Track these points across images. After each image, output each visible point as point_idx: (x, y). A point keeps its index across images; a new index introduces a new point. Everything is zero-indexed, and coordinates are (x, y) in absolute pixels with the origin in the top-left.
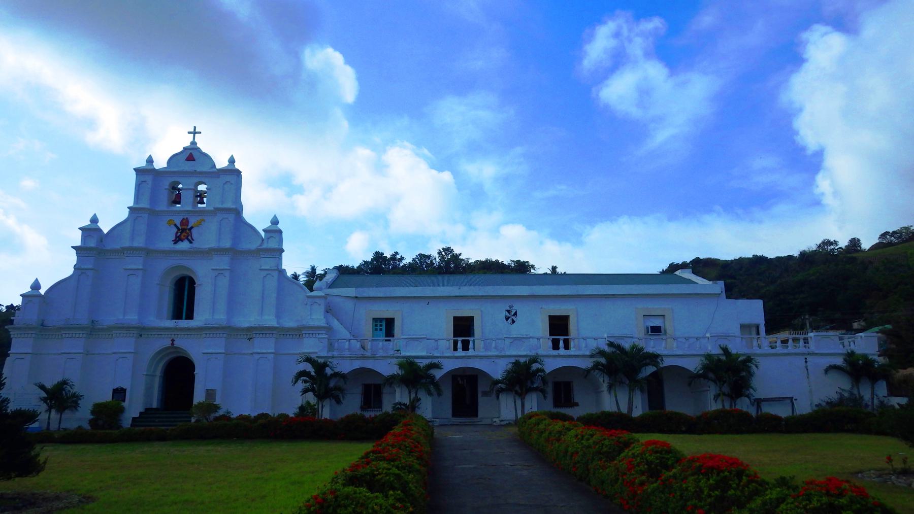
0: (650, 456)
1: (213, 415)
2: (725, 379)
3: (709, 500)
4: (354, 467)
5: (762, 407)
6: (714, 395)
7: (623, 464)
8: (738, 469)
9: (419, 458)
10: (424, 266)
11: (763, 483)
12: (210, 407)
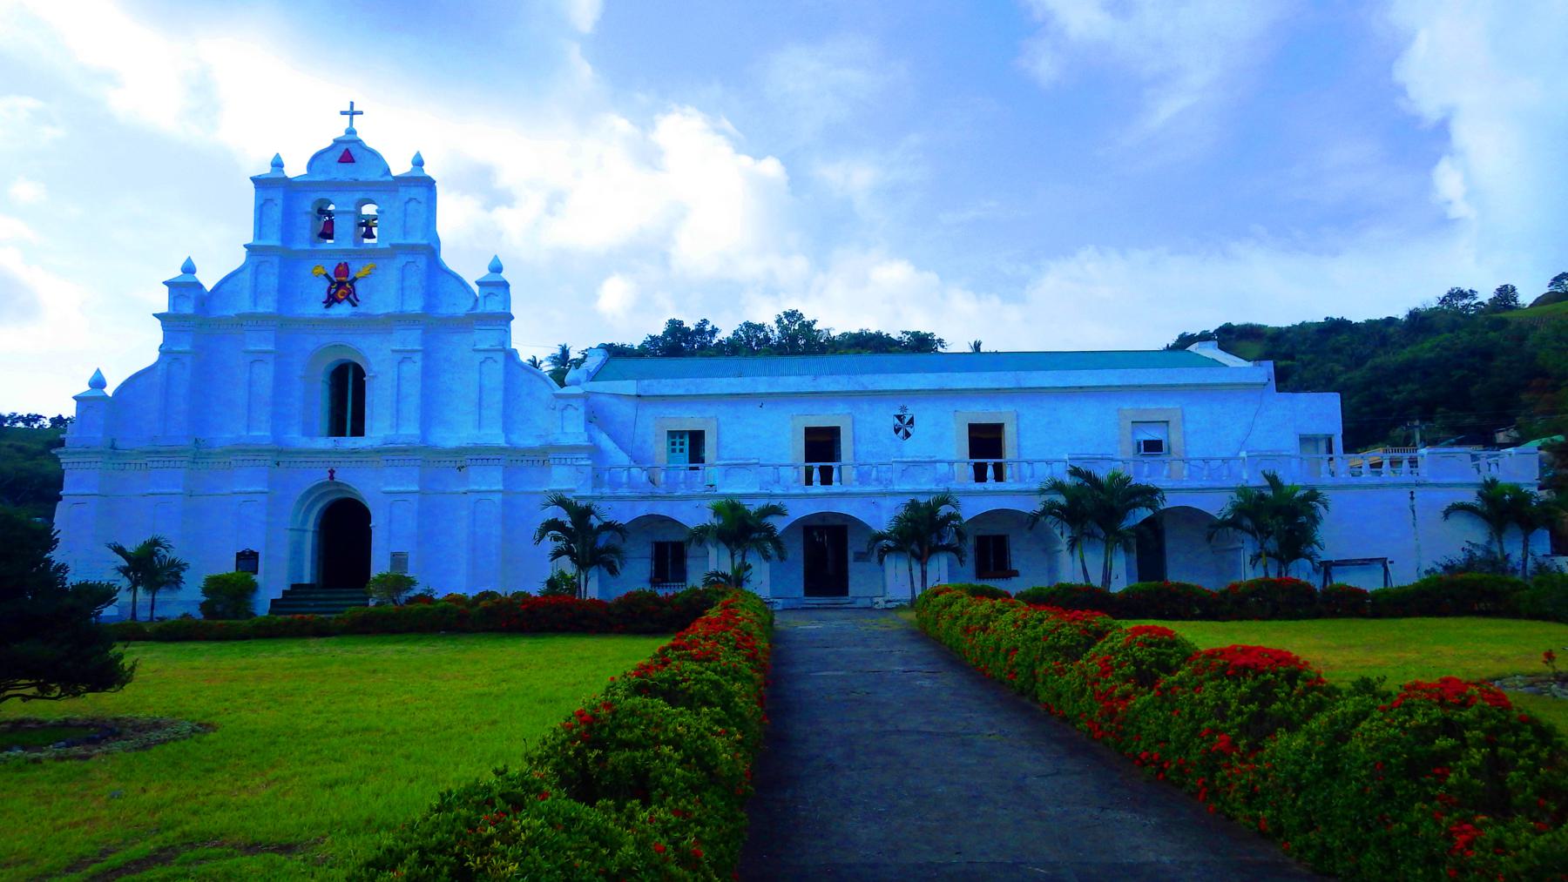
0: (1139, 650)
1: (404, 596)
2: (1270, 529)
3: (1239, 719)
4: (643, 670)
5: (1333, 575)
6: (1251, 556)
7: (1093, 665)
8: (1291, 668)
9: (751, 658)
10: (754, 344)
11: (1332, 692)
12: (399, 583)
